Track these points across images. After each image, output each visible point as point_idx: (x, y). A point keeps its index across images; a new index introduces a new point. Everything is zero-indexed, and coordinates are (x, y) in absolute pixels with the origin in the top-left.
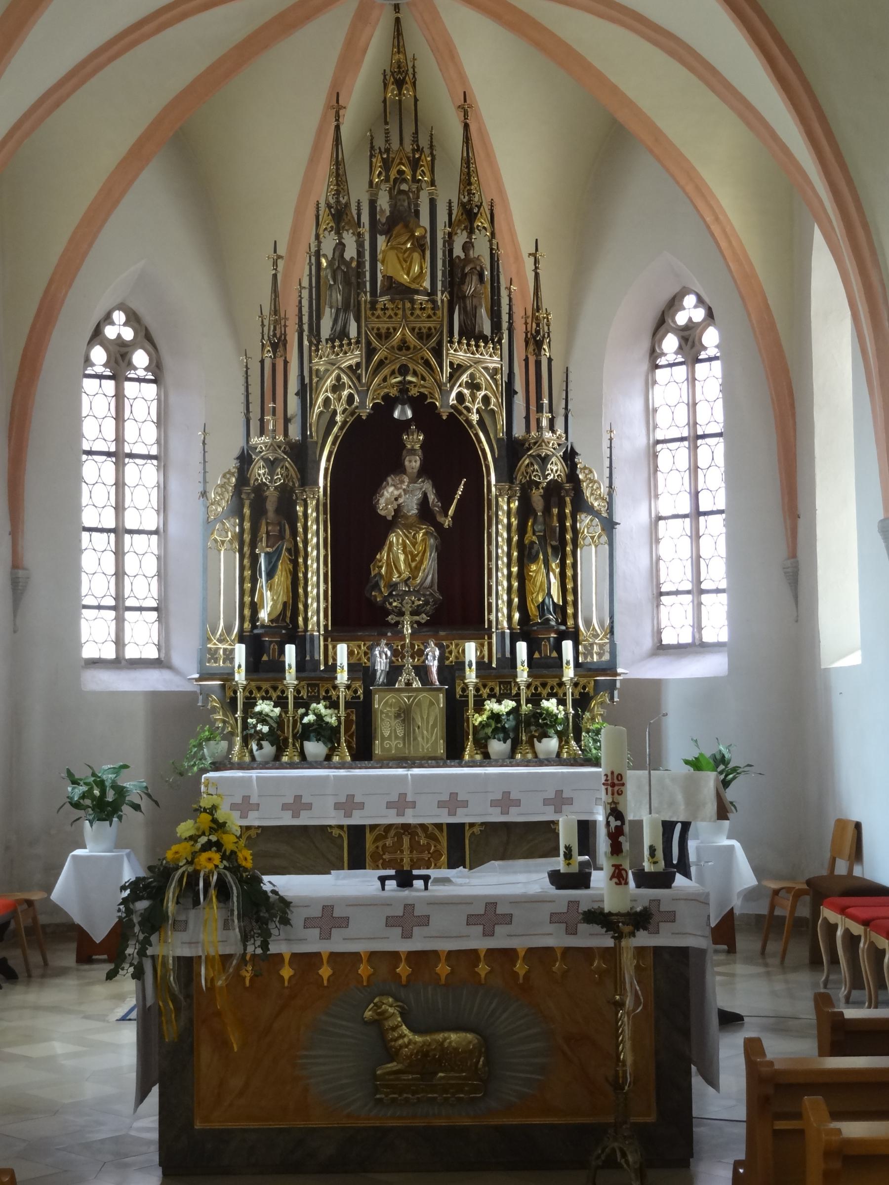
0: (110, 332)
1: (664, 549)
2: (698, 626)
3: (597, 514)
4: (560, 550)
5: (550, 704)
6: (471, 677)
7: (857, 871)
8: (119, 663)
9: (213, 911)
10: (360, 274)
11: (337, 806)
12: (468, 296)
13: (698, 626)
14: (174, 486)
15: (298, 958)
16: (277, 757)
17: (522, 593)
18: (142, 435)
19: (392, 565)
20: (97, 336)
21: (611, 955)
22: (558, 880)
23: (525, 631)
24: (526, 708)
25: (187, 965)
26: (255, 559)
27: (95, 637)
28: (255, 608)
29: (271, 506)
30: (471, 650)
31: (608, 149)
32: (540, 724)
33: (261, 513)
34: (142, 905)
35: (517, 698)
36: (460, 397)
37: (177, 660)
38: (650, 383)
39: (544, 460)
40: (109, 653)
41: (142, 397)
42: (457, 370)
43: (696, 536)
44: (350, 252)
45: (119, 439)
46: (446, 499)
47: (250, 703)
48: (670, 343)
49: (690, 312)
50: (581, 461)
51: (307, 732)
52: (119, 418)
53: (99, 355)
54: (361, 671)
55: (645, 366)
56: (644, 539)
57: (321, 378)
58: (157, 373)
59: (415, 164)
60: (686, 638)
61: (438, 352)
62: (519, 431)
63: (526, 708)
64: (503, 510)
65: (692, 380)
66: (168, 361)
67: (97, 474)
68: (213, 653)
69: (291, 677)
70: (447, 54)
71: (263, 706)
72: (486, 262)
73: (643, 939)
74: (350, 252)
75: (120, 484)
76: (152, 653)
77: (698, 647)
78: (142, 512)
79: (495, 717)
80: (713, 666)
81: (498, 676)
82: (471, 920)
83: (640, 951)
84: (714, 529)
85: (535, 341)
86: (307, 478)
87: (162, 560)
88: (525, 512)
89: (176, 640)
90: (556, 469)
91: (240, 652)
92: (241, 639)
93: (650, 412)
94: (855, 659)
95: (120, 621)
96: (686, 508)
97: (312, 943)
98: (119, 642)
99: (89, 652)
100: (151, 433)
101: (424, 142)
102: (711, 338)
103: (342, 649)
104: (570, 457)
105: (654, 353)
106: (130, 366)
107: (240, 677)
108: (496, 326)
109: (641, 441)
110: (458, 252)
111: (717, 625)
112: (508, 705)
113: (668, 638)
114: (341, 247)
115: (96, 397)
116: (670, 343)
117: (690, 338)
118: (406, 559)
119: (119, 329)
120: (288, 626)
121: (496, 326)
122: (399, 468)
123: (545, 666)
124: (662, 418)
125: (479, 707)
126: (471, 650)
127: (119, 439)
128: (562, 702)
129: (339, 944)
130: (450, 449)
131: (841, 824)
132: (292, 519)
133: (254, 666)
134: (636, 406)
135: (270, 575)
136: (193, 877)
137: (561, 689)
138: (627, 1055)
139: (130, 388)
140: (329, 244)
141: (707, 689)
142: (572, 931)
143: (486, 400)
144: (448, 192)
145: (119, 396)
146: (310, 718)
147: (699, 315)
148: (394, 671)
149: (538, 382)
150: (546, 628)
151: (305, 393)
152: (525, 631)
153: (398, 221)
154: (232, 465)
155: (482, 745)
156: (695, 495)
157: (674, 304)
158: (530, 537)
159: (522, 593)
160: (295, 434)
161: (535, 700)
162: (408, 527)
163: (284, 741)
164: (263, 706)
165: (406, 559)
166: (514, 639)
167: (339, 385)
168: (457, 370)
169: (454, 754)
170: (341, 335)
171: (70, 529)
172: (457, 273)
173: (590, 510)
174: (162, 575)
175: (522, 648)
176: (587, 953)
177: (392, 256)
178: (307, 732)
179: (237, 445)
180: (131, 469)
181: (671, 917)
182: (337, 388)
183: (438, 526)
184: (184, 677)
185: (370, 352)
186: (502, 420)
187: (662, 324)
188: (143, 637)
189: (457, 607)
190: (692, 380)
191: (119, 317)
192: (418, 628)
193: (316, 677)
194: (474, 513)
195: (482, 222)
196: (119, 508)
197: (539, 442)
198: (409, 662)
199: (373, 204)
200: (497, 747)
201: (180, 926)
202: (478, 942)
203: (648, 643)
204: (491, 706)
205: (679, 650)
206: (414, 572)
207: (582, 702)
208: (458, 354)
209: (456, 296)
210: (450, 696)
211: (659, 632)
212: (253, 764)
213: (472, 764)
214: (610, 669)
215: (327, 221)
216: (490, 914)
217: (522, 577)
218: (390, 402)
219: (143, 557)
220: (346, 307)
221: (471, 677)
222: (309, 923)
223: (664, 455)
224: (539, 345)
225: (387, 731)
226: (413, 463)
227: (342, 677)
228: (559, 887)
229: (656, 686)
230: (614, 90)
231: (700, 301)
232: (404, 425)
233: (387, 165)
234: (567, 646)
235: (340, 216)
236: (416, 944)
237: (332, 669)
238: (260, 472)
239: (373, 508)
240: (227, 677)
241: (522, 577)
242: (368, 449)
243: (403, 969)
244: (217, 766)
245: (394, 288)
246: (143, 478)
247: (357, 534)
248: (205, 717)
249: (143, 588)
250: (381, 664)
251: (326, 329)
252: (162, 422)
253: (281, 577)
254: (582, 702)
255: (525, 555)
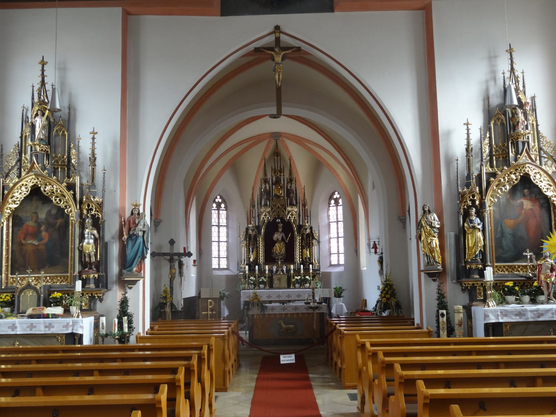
0: (217, 200)
1: (332, 244)
2: (339, 261)
3: (316, 240)
4: (309, 247)
5: (307, 277)
6: (292, 272)
7: (366, 309)
8: (219, 269)
9: (256, 308)
10: (270, 194)
11: (267, 297)
12: (291, 197)
13: (339, 261)
14: (230, 232)
15: (268, 314)
16: (254, 288)
17: (302, 255)
18: (223, 221)
19: (276, 250)
20: (214, 201)
21: (313, 314)
22: (306, 303)
23: (303, 263)
24: (303, 278)
25: (253, 315)
26: (249, 249)
27: (215, 265)
28: (249, 258)
29: (252, 238)
30: (292, 267)
31: (318, 167)
32: (306, 281)
33: (251, 240)
34: (246, 307)
35: (301, 276)
36: (290, 217)
37: (231, 268)
38: (329, 210)
39: (306, 229)
40: (217, 267)
41: (223, 213)
42: (289, 212)
43: (338, 242)
44: (268, 188)
45: (219, 222)
46: (287, 237)
47: (249, 277)
48: (333, 202)
49: (336, 195)
50: (313, 229)
51: (260, 283)
52: (219, 218)
53: (214, 205)
54: (271, 271)
55: (327, 206)
56: (327, 243)
57: (262, 213)
58: (226, 208)
59: (280, 172)
60: (336, 263)
61: (285, 209)
62: (301, 223)
63: (303, 278)
64: (298, 239)
65: (337, 210)
66: (228, 206)
67: (214, 230)
68: (242, 267)
69: (257, 272)
70: (286, 148)
71: (252, 278)
72: (294, 189)
73: (317, 311)
74: (268, 188)
75: (219, 232)
76: (226, 267)
77: (339, 265)
78: (223, 238)
79: (297, 280)
80: (341, 269)
81: (297, 272)
82: (293, 309)
83: (317, 313)
84: (341, 240)
85: (304, 205)
86: (259, 233)
87: (227, 247)
88: (302, 239)
89: (231, 264)
90: (308, 231)
91: (247, 267)
92: (247, 265)
93: (328, 216)
94: (365, 269)
95: (219, 260)
96: (336, 236)
97: (270, 312)
98: (219, 265)
99: (213, 267)
100: (225, 221)
101: (282, 167)
102: (340, 201)
103: (267, 267)
104: (311, 228)
105: (329, 204)
106: (221, 207)
107: (247, 272)
108: (296, 203)
109: (327, 222)
110: (289, 188)
111: (342, 262)
112: (299, 277)
113: (332, 263)
114: (266, 187)
115: (214, 214)
116: (333, 202)
117: (336, 201)
118: (279, 249)
119: (218, 200)
120: (256, 262)
121: (296, 203)
122: (278, 231)
123: (306, 270)
124: (331, 217)
125: (294, 278)
126: (292, 267)
127: (219, 222)
128: (310, 277)
129: (274, 312)
130: (288, 227)
131: (363, 300)
132: (257, 241)
133: (250, 270)
134: (326, 215)
135: (252, 252)
136: (253, 303)
137: (311, 273)
138: (315, 327)
139: (221, 212)
140: (263, 186)
141: (340, 273)
142: (307, 310)
143: (295, 217)
144: (287, 175)
145: (219, 214)
146: (261, 280)
147: (338, 196)
148: (277, 271)
149: (305, 214)
150: (306, 262)
151: (259, 216)
152: (303, 263)
153: (277, 182)
154: (245, 230)
155: (294, 285)
156: (338, 233)
157: (333, 194)
158: (303, 244)
159: (302, 255)
160: (257, 224)
161: (304, 276)
162: (279, 242)
163: (256, 284)
164: (252, 278)
165: (279, 249)
166: (301, 264)
167: (265, 215)
168: (289, 212)
169: (289, 287)
170: (266, 205)
171: (210, 242)
172: (289, 192)
173: (315, 239)
174: (227, 250)
175: (302, 266)
176: (310, 313)
177: (276, 190)
178: (260, 283)
179: (246, 226)
180: (221, 228)
181: (322, 308)
182: (265, 215)
183: (285, 242)
184: (234, 271)
185: (272, 209)
186: (298, 221)
187: (331, 198)
188: (224, 264)
189: (289, 258)
190: (337, 210)
191: (218, 197)
192: (282, 262)
193: (262, 272)
194: (292, 240)
195: (294, 182)
196: (219, 237)
197: (305, 226)
198: (280, 269)
199: (272, 179)
200: (297, 285)
201: (252, 310)
202: (294, 312)
203: (328, 264)
204: (296, 277)
205: (335, 266)
206: (281, 251)
207: (314, 277)
208: (289, 209)
209: (288, 195)
210: (288, 275)
211: (331, 262)
212: (250, 289)
213: (292, 289)
214: (319, 270)
215: (263, 182)
216: (296, 308)
217: (302, 252)
218: (276, 219)
219: (223, 247)
220: (267, 199)
221: (292, 272)
222: (270, 309)
223: (332, 225)
224: (305, 206)
225: (276, 282)
226: (280, 230)
227: (267, 272)
228: (351, 400)
229: (329, 273)
230: (319, 156)
231: (338, 194)
232: (279, 223)
233: (275, 172)
234: (311, 266)
235: (266, 181)
236: (285, 312)
237: (265, 270)
238: (250, 232)
239: (273, 239)
240: (245, 272)
241: (302, 252)
242: (271, 227)
243: (283, 316)
244: (243, 289)
245: (278, 197)
246: (223, 230)
247: (269, 244)
248: (240, 280)
249: (223, 254)
250: (274, 269)
251: (263, 204)
252: (227, 218)
253: (255, 252)
254: (314, 277)
255: (302, 248)
